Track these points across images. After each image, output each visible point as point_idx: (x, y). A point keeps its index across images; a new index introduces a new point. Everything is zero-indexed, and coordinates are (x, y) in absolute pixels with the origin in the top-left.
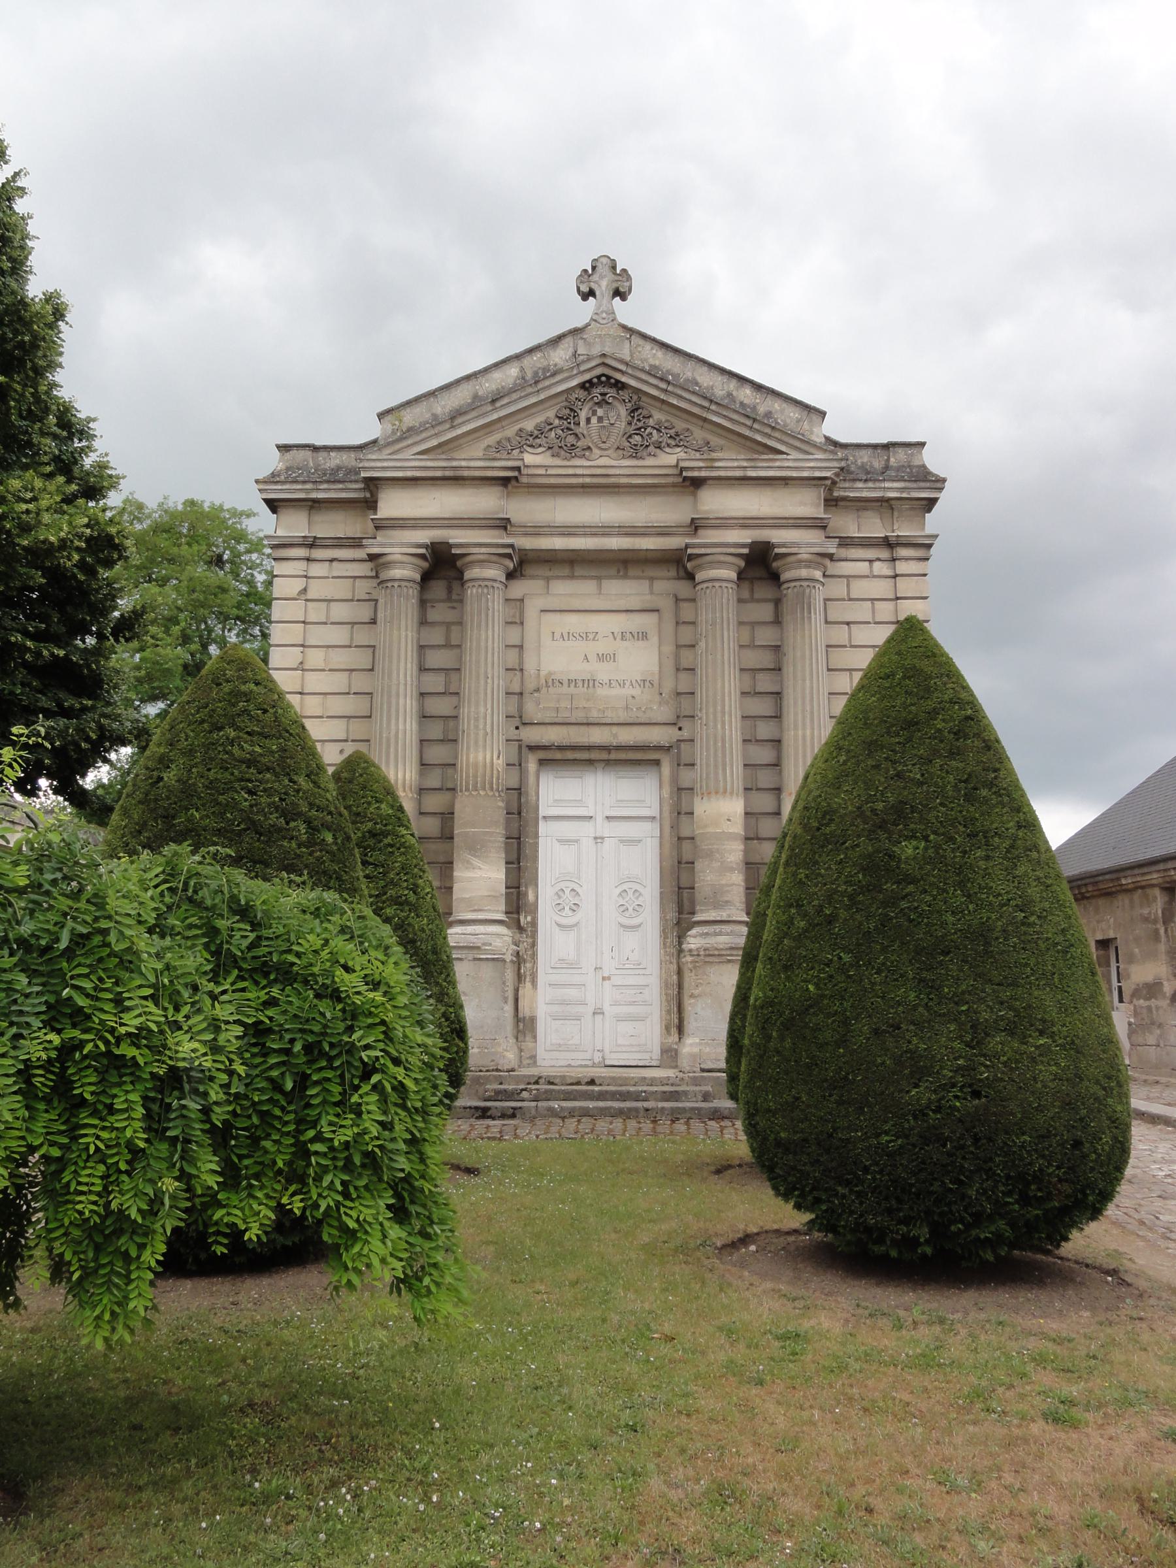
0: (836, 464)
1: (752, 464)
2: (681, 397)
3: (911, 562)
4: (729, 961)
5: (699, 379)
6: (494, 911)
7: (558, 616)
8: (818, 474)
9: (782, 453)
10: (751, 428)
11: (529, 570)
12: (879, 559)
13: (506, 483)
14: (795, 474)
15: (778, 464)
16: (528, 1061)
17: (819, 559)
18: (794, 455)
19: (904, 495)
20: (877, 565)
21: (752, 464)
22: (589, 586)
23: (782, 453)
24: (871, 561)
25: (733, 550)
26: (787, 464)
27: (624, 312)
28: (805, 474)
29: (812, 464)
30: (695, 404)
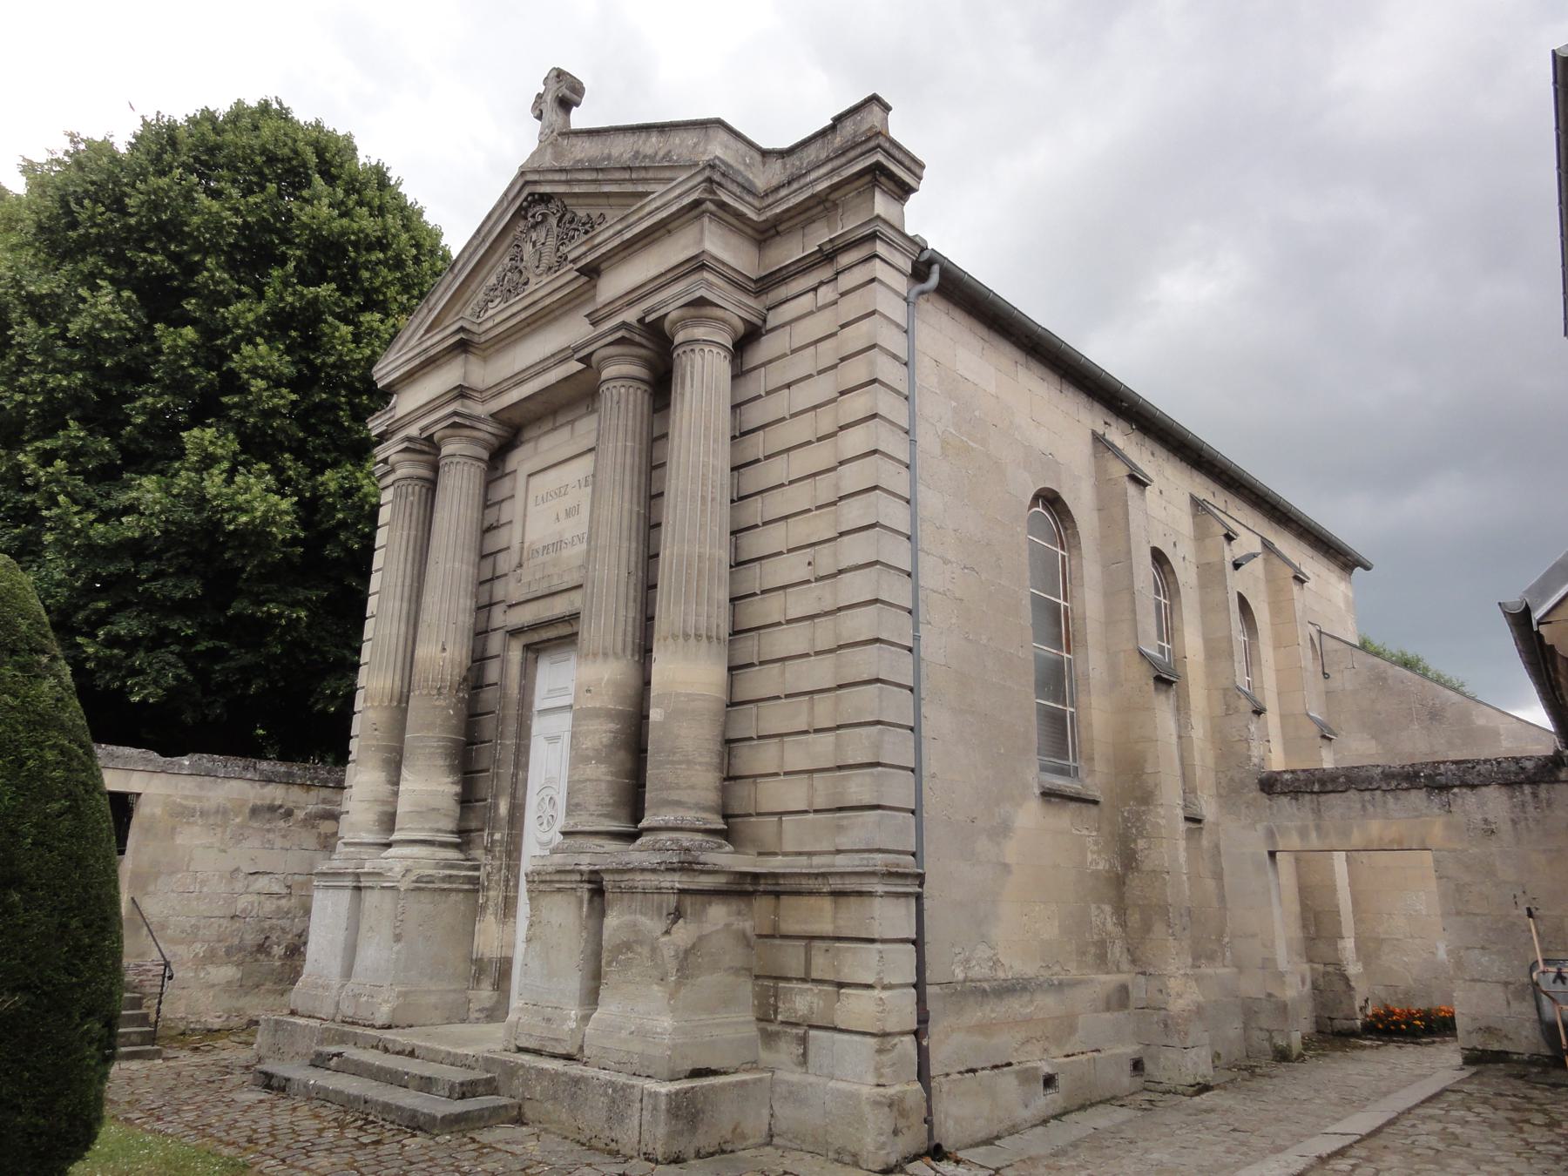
0: (700, 178)
1: (625, 224)
2: (580, 181)
3: (855, 270)
4: (559, 890)
5: (615, 152)
6: (411, 829)
7: (541, 475)
8: (686, 201)
9: (647, 194)
10: (631, 180)
11: (527, 435)
12: (822, 283)
13: (463, 346)
14: (664, 214)
15: (647, 209)
16: (477, 1015)
17: (692, 311)
18: (660, 188)
19: (836, 179)
20: (822, 290)
21: (625, 224)
22: (564, 433)
23: (647, 194)
24: (815, 289)
25: (610, 339)
26: (653, 206)
27: (580, 118)
28: (674, 208)
29: (678, 192)
30: (560, 182)
